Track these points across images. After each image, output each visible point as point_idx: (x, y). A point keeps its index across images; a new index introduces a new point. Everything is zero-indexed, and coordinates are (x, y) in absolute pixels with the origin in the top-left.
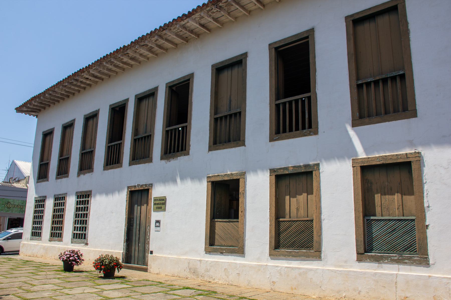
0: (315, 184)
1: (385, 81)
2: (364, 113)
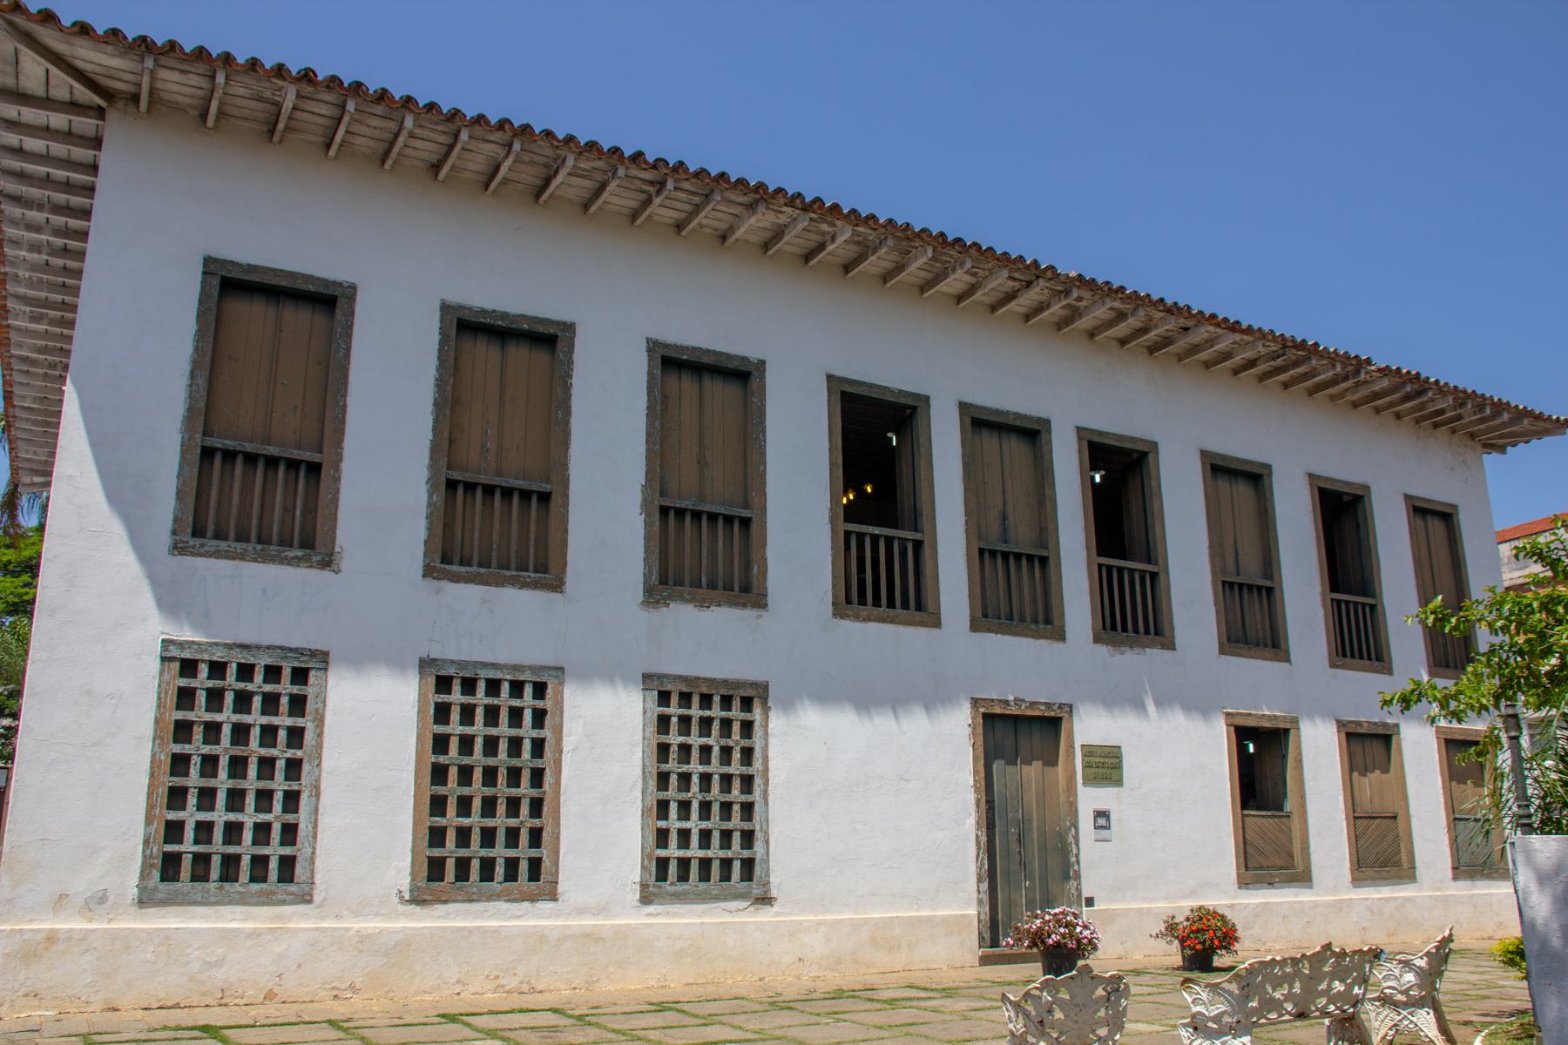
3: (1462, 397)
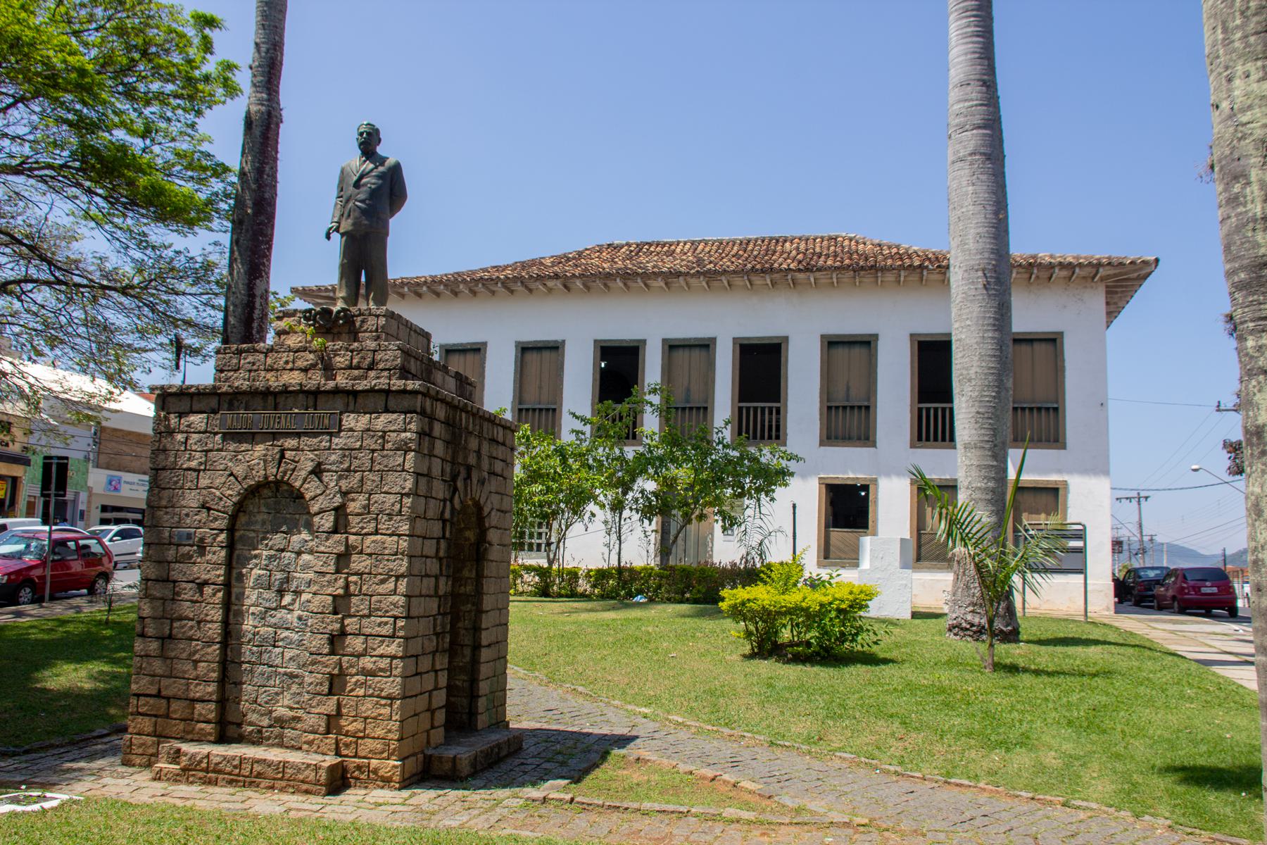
1: (1039, 409)
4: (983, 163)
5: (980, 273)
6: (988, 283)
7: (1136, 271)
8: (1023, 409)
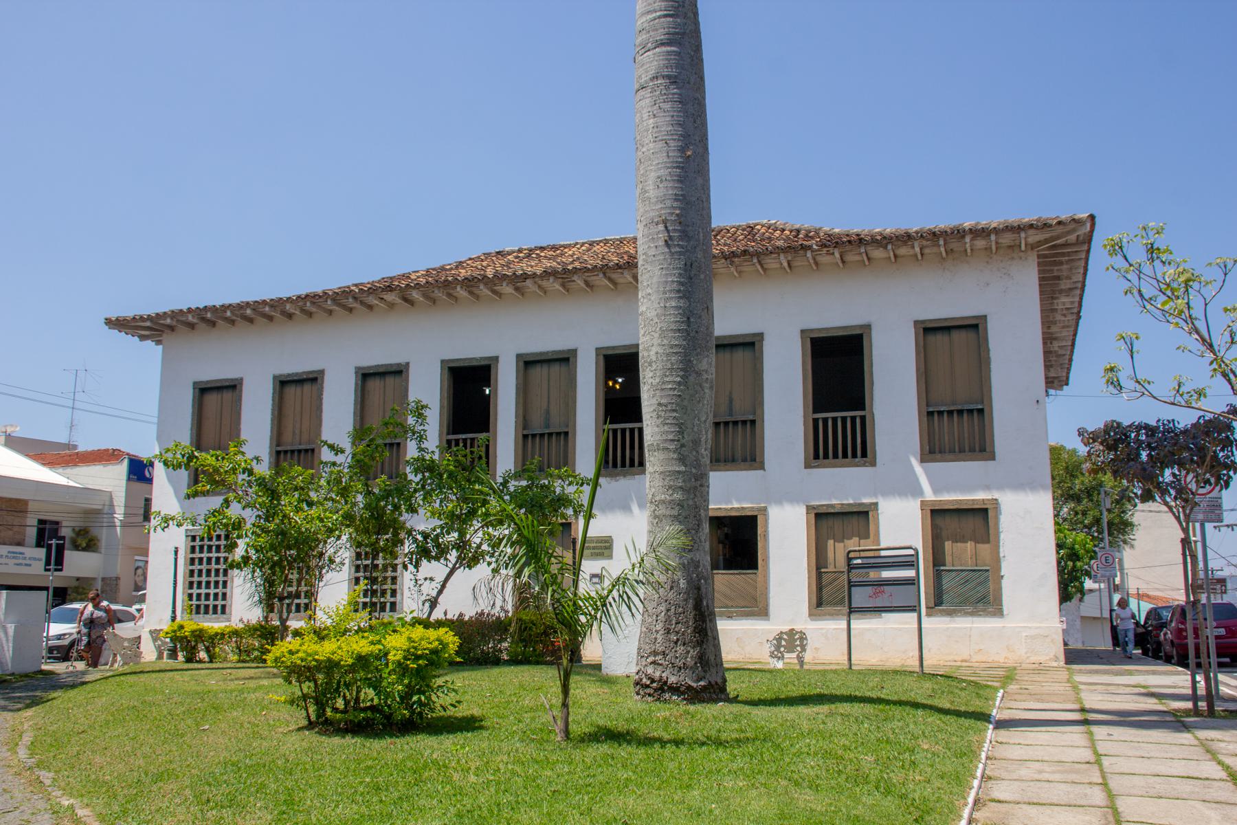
0: (872, 526)
1: (960, 412)
2: (933, 450)
3: (241, 306)
4: (667, 88)
5: (661, 227)
6: (670, 238)
7: (1069, 233)
8: (940, 413)
